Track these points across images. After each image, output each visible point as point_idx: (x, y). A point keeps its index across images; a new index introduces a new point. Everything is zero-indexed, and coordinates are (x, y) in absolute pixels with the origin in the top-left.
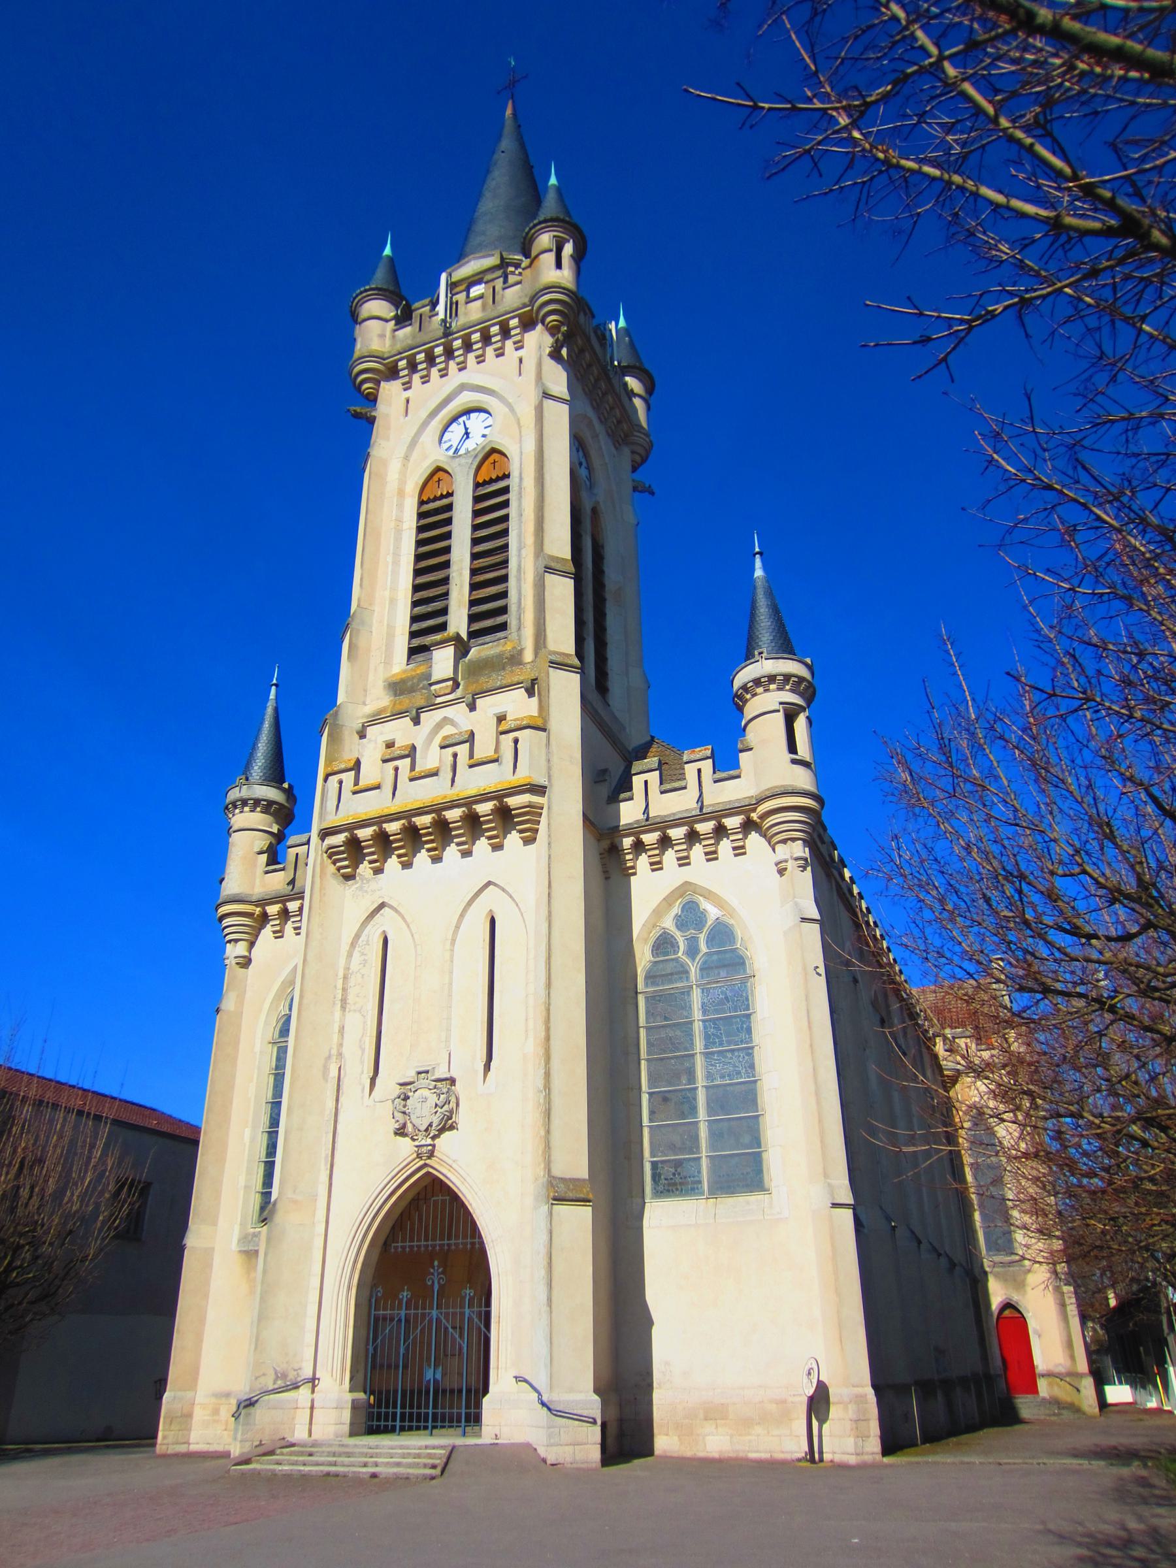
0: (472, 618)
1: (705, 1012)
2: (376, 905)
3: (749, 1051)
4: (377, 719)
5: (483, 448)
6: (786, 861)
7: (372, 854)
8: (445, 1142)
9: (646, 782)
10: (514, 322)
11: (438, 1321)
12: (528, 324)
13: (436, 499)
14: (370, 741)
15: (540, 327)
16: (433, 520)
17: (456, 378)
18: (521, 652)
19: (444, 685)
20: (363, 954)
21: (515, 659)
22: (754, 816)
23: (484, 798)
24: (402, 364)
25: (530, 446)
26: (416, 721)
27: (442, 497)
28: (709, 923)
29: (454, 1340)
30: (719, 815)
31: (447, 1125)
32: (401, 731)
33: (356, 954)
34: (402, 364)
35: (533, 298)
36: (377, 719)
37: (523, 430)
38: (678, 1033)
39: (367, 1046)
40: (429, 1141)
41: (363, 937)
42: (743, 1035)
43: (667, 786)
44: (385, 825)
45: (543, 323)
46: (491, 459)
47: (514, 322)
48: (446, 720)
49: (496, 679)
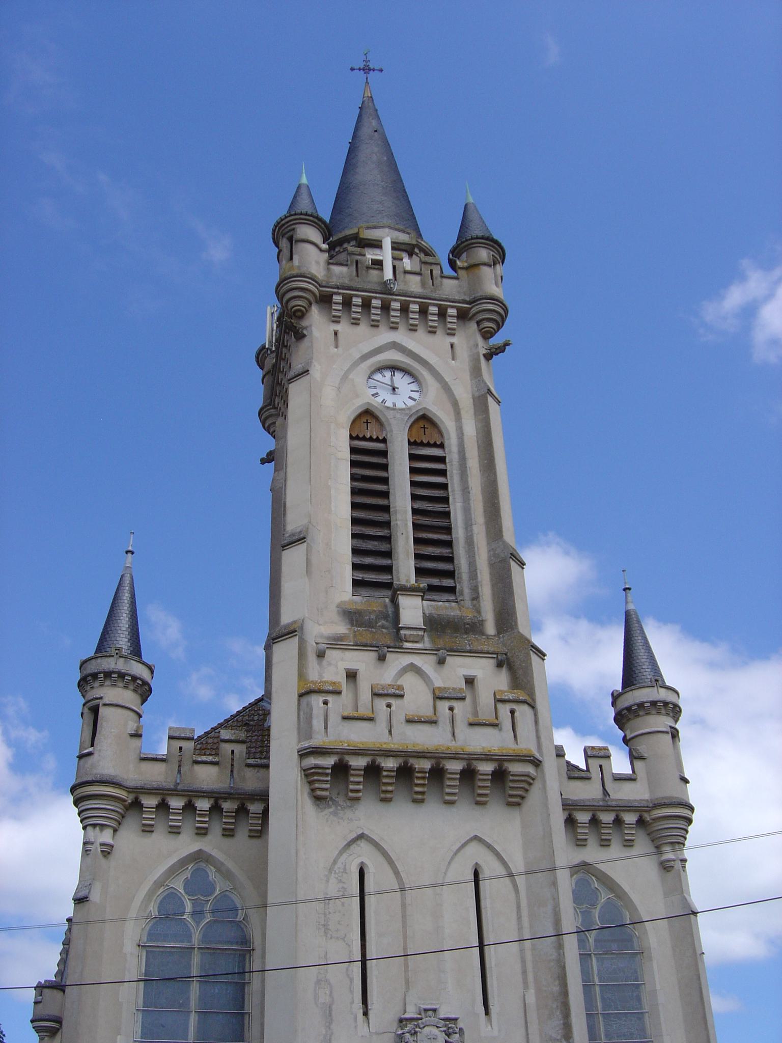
0: (419, 572)
2: (354, 835)
3: (640, 1016)
4: (337, 643)
6: (674, 860)
7: (358, 783)
10: (452, 311)
12: (463, 316)
13: (371, 439)
14: (330, 664)
16: (369, 463)
17: (401, 336)
18: (482, 622)
19: (415, 633)
20: (340, 881)
21: (475, 627)
22: (647, 817)
23: (487, 757)
24: (338, 298)
25: (470, 428)
26: (382, 658)
27: (377, 440)
28: (217, 892)
30: (620, 809)
32: (362, 661)
33: (333, 880)
34: (338, 298)
35: (472, 302)
36: (337, 643)
37: (463, 412)
39: (495, 982)
41: (339, 864)
44: (475, 763)
45: (478, 323)
46: (421, 424)
47: (452, 311)
48: (413, 668)
49: (465, 641)
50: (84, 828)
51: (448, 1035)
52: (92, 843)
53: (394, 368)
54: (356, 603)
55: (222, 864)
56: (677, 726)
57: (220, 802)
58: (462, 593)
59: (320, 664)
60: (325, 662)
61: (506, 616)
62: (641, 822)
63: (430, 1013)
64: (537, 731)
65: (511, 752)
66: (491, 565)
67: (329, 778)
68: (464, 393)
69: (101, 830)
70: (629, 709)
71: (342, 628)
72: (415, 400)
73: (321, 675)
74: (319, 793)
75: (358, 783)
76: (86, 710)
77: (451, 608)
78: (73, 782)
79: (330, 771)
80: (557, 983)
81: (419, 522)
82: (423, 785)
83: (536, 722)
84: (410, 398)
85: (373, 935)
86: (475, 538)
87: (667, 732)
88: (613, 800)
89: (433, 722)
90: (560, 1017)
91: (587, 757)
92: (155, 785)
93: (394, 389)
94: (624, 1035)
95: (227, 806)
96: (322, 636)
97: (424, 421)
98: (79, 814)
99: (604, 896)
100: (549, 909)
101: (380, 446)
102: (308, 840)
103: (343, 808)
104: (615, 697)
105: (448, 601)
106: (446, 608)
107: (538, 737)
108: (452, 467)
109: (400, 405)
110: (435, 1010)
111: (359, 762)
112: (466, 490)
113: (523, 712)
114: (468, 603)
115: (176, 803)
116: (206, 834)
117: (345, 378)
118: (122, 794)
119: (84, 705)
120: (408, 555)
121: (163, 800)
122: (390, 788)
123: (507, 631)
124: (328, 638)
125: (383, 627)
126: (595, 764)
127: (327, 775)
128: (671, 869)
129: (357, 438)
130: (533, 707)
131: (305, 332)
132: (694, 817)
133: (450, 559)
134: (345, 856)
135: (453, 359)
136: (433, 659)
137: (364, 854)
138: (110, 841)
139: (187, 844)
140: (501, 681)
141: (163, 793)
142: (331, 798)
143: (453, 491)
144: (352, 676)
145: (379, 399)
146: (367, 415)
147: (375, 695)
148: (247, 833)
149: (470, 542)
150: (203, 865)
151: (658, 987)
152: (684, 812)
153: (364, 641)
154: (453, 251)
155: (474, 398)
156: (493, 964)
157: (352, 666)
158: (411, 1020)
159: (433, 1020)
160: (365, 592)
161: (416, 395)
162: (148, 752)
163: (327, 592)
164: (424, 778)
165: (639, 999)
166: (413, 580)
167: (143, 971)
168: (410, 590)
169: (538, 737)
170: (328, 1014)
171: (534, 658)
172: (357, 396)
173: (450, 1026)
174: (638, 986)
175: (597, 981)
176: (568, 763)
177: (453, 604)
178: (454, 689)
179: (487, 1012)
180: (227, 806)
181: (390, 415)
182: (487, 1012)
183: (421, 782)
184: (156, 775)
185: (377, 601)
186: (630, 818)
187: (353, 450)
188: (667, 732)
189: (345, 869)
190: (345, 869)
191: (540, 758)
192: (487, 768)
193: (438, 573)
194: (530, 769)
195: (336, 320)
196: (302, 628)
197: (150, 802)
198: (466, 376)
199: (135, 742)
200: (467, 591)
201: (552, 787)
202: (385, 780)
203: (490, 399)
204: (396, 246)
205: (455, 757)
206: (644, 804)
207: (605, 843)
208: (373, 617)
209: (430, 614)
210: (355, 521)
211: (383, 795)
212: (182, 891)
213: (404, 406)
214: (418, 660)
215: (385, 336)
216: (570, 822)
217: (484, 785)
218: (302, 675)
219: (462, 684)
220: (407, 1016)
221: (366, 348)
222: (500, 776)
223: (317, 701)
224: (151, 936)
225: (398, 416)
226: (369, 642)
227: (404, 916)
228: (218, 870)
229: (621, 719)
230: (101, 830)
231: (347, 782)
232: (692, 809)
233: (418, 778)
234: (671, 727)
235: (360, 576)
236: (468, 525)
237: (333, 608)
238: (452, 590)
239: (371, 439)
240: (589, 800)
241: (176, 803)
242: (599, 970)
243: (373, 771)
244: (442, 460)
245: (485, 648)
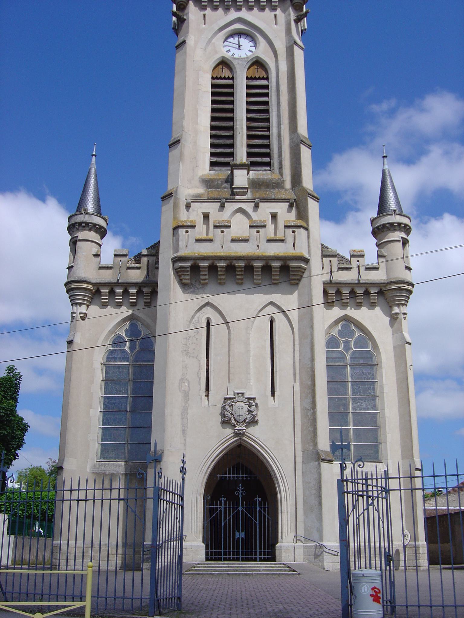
0: (249, 155)
1: (352, 378)
2: (204, 303)
3: (374, 399)
4: (197, 199)
5: (252, 59)
6: (398, 314)
7: (205, 275)
8: (252, 431)
9: (330, 261)
11: (242, 511)
13: (225, 78)
14: (193, 210)
17: (244, 14)
18: (283, 182)
21: (279, 185)
23: (277, 258)
26: (222, 206)
27: (229, 78)
28: (142, 335)
29: (251, 520)
31: (253, 422)
32: (212, 208)
36: (197, 199)
38: (339, 387)
40: (244, 428)
42: (370, 391)
43: (343, 266)
50: (72, 305)
51: (250, 406)
52: (75, 313)
53: (239, 33)
54: (211, 175)
55: (144, 320)
56: (408, 238)
57: (142, 288)
58: (273, 166)
59: (188, 211)
60: (190, 210)
62: (381, 293)
63: (240, 395)
64: (308, 243)
65: (290, 255)
66: (291, 148)
67: (189, 273)
68: (281, 46)
69: (80, 306)
70: (378, 228)
71: (201, 190)
72: (252, 52)
73: (188, 217)
74: (184, 281)
75: (205, 275)
76: (71, 243)
77: (267, 174)
78: (66, 281)
79: (189, 269)
80: (310, 379)
81: (250, 125)
82: (241, 275)
83: (308, 238)
84: (249, 51)
85: (212, 355)
86: (282, 132)
87: (399, 241)
88: (364, 280)
89: (246, 240)
90: (311, 397)
91: (351, 256)
92: (106, 281)
93: (239, 46)
94: (364, 409)
95: (145, 290)
96: (189, 195)
97: (258, 63)
98: (69, 298)
99: (358, 333)
100: (309, 339)
102: (179, 307)
103: (198, 289)
104: (373, 221)
105: (265, 170)
106: (263, 175)
108: (273, 92)
109: (243, 56)
110: (243, 394)
111: (204, 264)
114: (276, 170)
115: (119, 290)
116: (136, 305)
117: (209, 41)
118: (90, 287)
119: (70, 241)
120: (242, 146)
121: (112, 289)
122: (223, 277)
123: (296, 186)
124: (193, 196)
125: (225, 188)
126: (354, 260)
127: (188, 271)
129: (217, 78)
130: (307, 229)
131: (185, 17)
133: (268, 146)
134: (199, 314)
135: (276, 24)
136: (253, 204)
137: (208, 312)
138: (85, 311)
139: (125, 312)
140: (292, 217)
141: (112, 286)
142: (192, 284)
143: (272, 105)
144: (274, 216)
145: (230, 54)
146: (224, 63)
147: (287, 227)
148: (143, 304)
150: (135, 322)
151: (384, 383)
153: (213, 196)
155: (287, 48)
156: (278, 370)
158: (230, 399)
159: (242, 398)
160: (217, 168)
161: (253, 49)
162: (104, 263)
163: (193, 170)
164: (241, 271)
165: (374, 389)
167: (104, 377)
168: (241, 166)
170: (186, 396)
172: (216, 53)
174: (374, 383)
175: (350, 379)
177: (268, 172)
178: (260, 221)
179: (273, 394)
180: (145, 290)
181: (235, 63)
182: (273, 394)
183: (240, 273)
184: (107, 276)
185: (223, 173)
188: (399, 241)
189: (198, 321)
190: (198, 321)
191: (309, 258)
192: (276, 264)
193: (260, 155)
195: (204, 8)
196: (176, 191)
197: (105, 290)
198: (283, 35)
199: (97, 259)
201: (318, 274)
202: (219, 273)
203: (296, 48)
205: (258, 259)
206: (383, 282)
207: (359, 306)
208: (219, 182)
209: (253, 179)
210: (213, 128)
211: (219, 281)
212: (124, 335)
213: (245, 56)
214: (243, 206)
215: (233, 15)
216: (325, 292)
217: (258, 274)
218: (175, 218)
220: (228, 396)
221: (222, 23)
223: (182, 232)
224: (108, 359)
225: (241, 62)
226: (216, 197)
227: (229, 345)
228: (143, 324)
229: (375, 233)
230: (80, 306)
231: (200, 275)
233: (238, 271)
234: (402, 238)
235: (214, 159)
237: (197, 179)
238: (268, 164)
239: (225, 78)
240: (349, 280)
241: (119, 290)
242: (352, 374)
243: (213, 269)
244: (266, 87)
245: (283, 197)
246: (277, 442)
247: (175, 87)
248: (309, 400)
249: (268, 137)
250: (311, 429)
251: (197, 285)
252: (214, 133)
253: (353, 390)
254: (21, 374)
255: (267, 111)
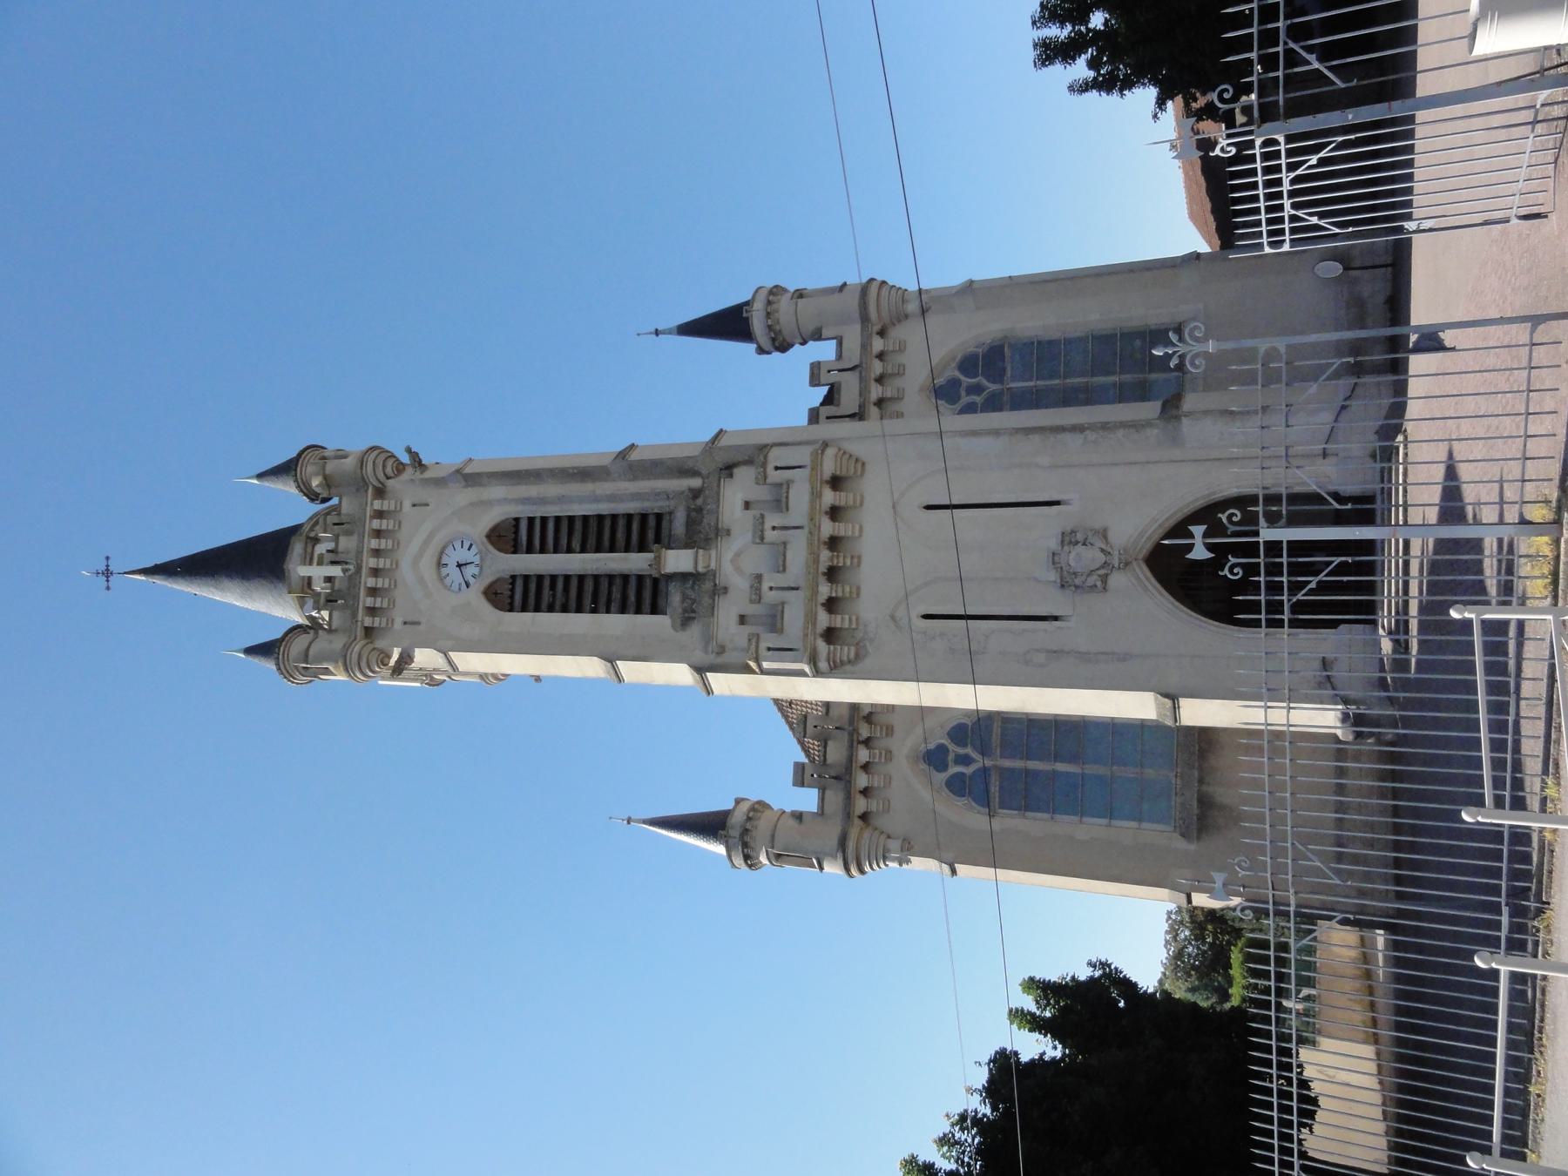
0: (642, 548)
3: (1069, 342)
15: (390, 483)
18: (691, 490)
21: (696, 493)
23: (816, 495)
25: (498, 491)
27: (513, 584)
31: (1104, 534)
56: (792, 290)
61: (682, 469)
66: (635, 478)
70: (774, 340)
71: (695, 630)
74: (852, 655)
91: (818, 385)
101: (519, 583)
104: (761, 351)
107: (799, 444)
108: (539, 512)
112: (561, 499)
113: (776, 457)
114: (672, 503)
126: (824, 378)
128: (927, 304)
132: (880, 278)
133: (629, 517)
140: (744, 475)
149: (612, 498)
152: (874, 286)
154: (312, 500)
157: (734, 619)
165: (1050, 342)
166: (650, 556)
169: (799, 444)
171: (724, 442)
173: (1069, 539)
176: (822, 404)
180: (865, 732)
184: (835, 797)
186: (878, 345)
187: (524, 609)
193: (645, 530)
194: (830, 452)
200: (661, 503)
203: (467, 470)
204: (308, 560)
219: (750, 513)
222: (836, 482)
229: (783, 347)
232: (872, 280)
236: (597, 499)
239: (512, 590)
243: (831, 605)
246: (1143, 481)
247: (579, 675)
248: (1067, 437)
249: (614, 517)
250: (1120, 433)
251: (859, 635)
252: (602, 606)
253: (1051, 377)
254: (944, 1127)
255: (571, 519)
